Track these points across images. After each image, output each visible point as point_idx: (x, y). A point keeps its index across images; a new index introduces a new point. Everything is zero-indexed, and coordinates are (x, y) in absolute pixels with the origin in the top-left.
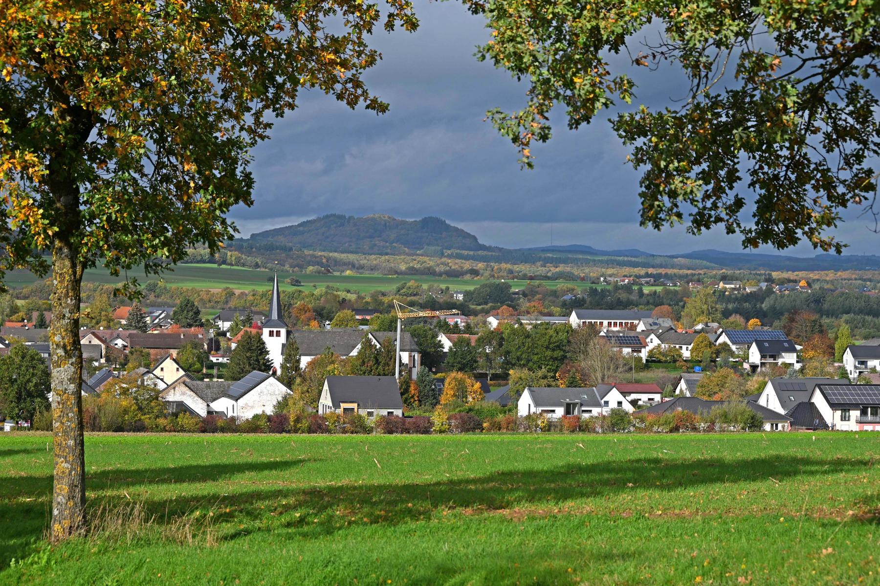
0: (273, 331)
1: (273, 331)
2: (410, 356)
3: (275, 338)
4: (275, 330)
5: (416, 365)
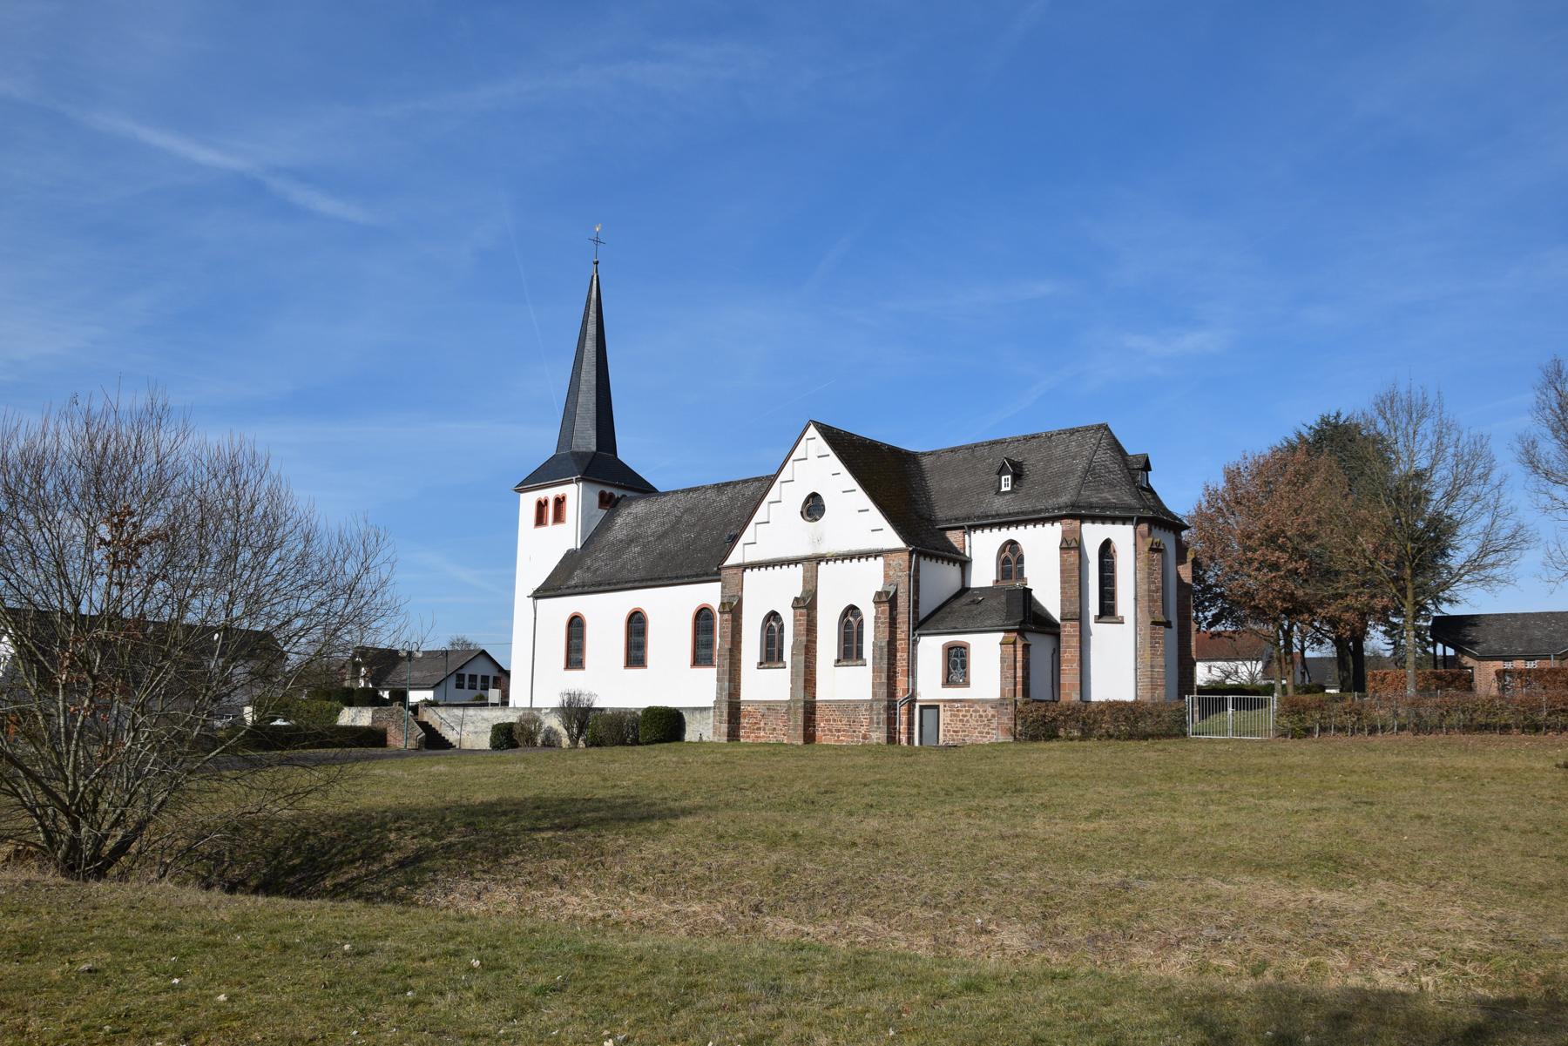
2: (1072, 546)
3: (550, 528)
4: (550, 494)
5: (1125, 601)
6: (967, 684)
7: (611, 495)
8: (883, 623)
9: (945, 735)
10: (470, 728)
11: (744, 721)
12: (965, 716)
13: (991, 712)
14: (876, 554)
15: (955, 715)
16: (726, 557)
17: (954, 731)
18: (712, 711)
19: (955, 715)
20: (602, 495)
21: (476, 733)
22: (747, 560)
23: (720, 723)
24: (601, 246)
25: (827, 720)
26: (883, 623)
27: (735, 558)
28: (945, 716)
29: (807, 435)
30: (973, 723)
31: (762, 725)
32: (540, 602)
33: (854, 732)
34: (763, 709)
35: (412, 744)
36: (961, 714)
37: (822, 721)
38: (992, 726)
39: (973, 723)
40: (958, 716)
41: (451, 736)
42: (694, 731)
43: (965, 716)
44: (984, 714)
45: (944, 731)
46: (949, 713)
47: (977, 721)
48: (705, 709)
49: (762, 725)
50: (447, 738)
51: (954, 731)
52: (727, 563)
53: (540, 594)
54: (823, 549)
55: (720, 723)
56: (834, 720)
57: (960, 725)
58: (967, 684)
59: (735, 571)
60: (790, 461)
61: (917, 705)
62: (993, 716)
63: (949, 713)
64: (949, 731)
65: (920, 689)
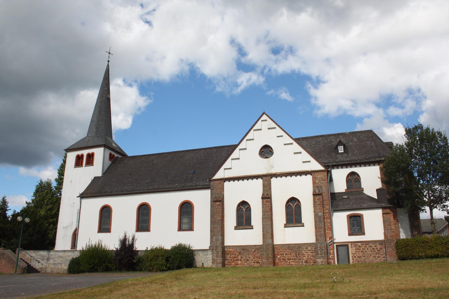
0: (82, 156)
1: (82, 156)
6: (364, 234)
7: (114, 156)
8: (318, 205)
9: (353, 259)
10: (51, 261)
11: (228, 257)
12: (364, 249)
13: (379, 246)
14: (257, 177)
15: (358, 249)
16: (214, 175)
17: (358, 257)
18: (210, 252)
19: (358, 249)
20: (110, 154)
21: (55, 264)
22: (226, 176)
23: (217, 257)
24: (111, 56)
25: (281, 254)
26: (318, 205)
27: (220, 174)
28: (351, 250)
29: (262, 119)
30: (369, 252)
31: (239, 257)
32: (84, 201)
33: (300, 259)
34: (239, 250)
35: (20, 272)
36: (361, 248)
37: (279, 255)
38: (381, 253)
39: (369, 252)
40: (360, 249)
41: (37, 266)
42: (199, 259)
43: (364, 249)
44: (375, 248)
45: (352, 257)
46: (354, 248)
47: (371, 251)
48: (205, 250)
49: (239, 257)
50: (34, 267)
51: (358, 257)
52: (215, 177)
53: (83, 196)
54: (273, 171)
55: (217, 257)
56: (286, 254)
57: (361, 254)
58: (364, 234)
59: (219, 182)
60: (252, 130)
61: (335, 245)
62: (381, 248)
63: (354, 248)
64: (355, 257)
65: (335, 237)
